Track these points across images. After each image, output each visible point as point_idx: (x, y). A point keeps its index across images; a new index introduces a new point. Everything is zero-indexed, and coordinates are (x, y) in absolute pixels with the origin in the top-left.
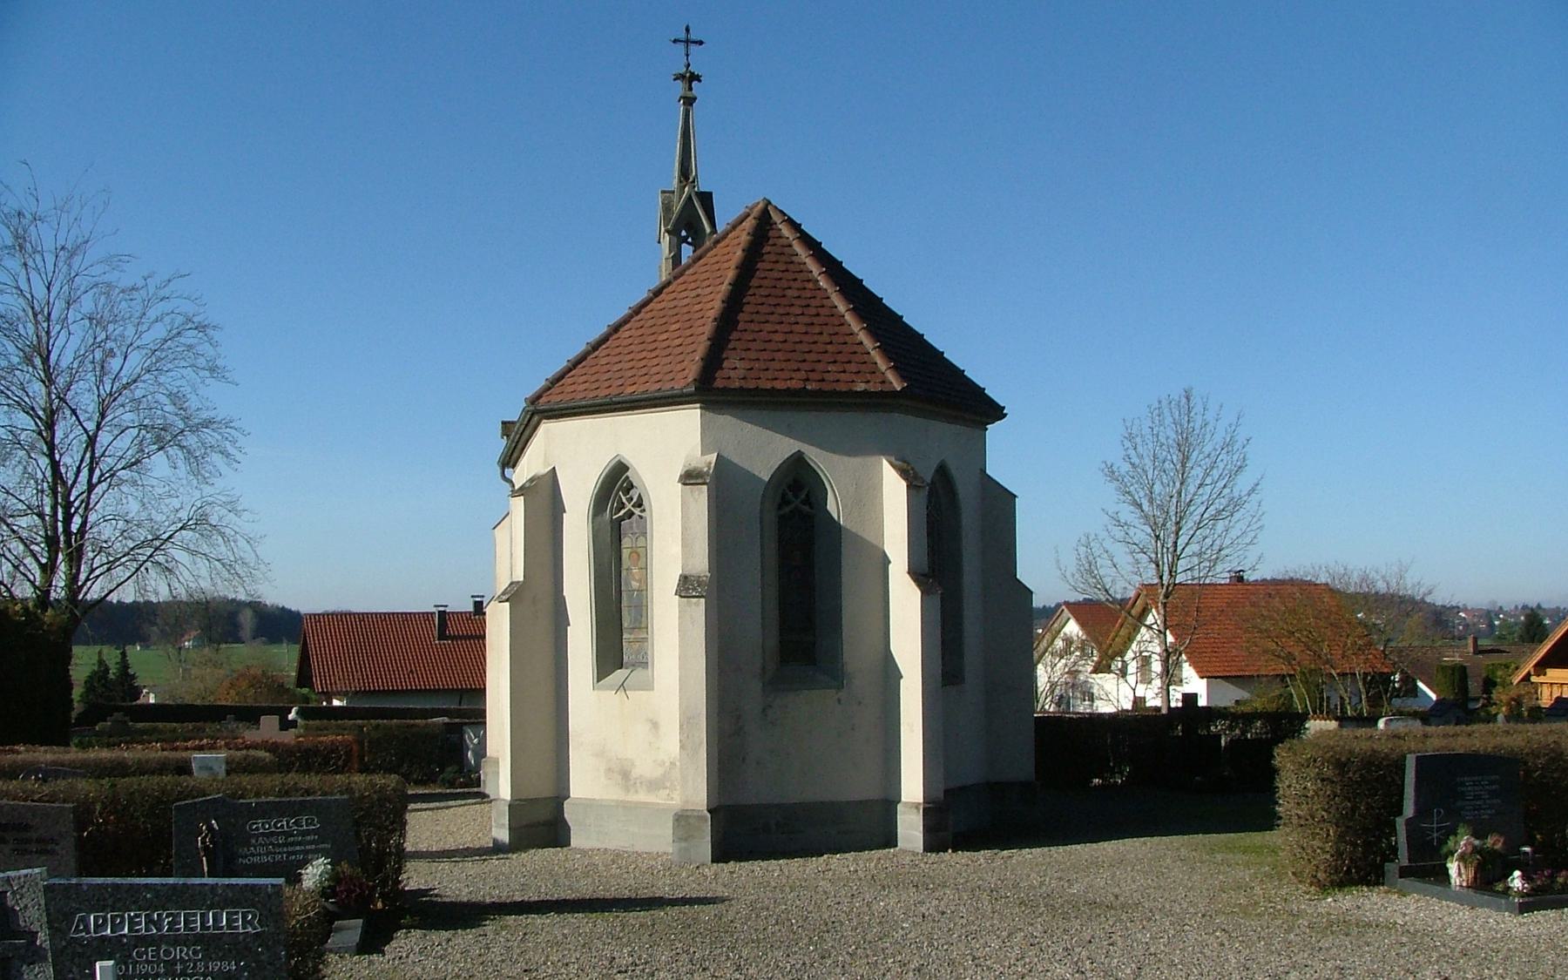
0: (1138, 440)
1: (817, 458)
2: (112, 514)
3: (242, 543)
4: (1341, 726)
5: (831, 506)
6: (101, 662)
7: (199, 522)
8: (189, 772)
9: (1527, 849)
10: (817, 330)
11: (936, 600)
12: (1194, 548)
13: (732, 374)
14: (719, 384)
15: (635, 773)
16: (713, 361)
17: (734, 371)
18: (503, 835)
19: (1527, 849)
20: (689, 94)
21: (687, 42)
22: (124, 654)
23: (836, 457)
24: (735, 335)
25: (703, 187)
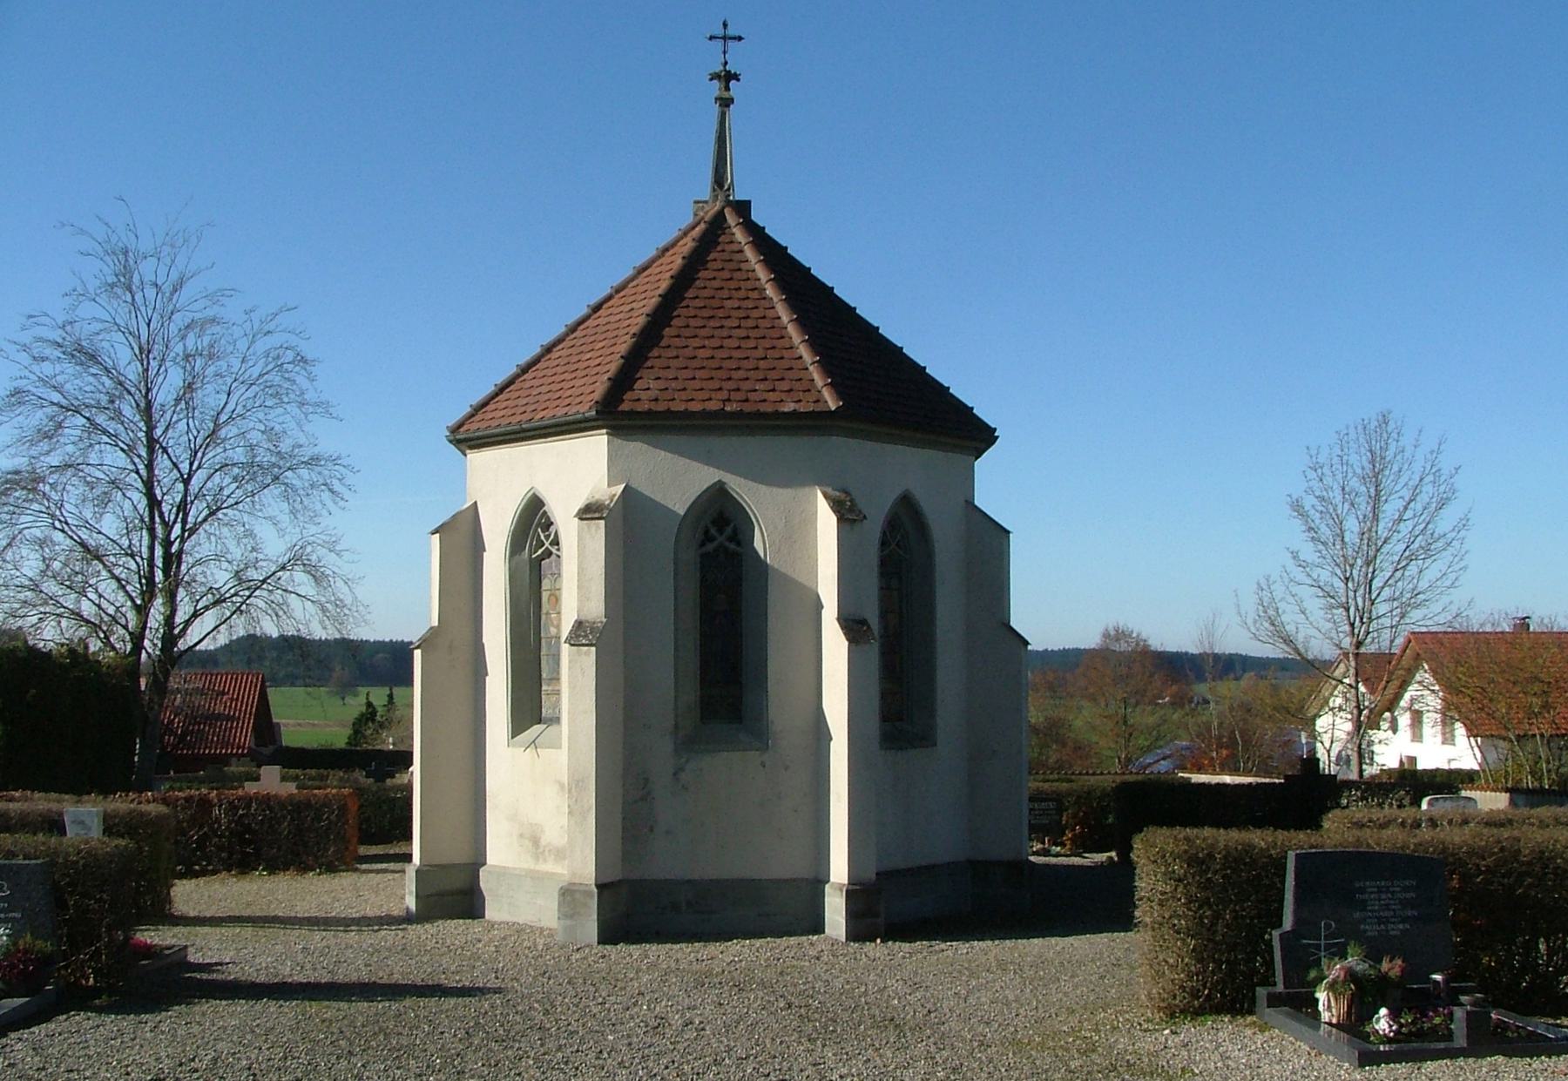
0: (1326, 470)
1: (744, 490)
2: (212, 559)
3: (340, 583)
4: (1512, 802)
5: (758, 544)
6: (369, 705)
7: (297, 559)
8: (63, 832)
9: (1438, 977)
10: (752, 343)
11: (873, 650)
12: (1386, 592)
13: (644, 395)
14: (625, 407)
15: (543, 842)
16: (623, 381)
17: (646, 392)
18: (411, 902)
19: (1438, 977)
20: (726, 95)
21: (725, 38)
22: (391, 696)
23: (763, 488)
24: (655, 352)
25: (739, 195)
